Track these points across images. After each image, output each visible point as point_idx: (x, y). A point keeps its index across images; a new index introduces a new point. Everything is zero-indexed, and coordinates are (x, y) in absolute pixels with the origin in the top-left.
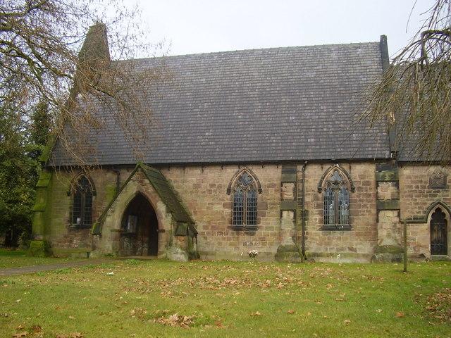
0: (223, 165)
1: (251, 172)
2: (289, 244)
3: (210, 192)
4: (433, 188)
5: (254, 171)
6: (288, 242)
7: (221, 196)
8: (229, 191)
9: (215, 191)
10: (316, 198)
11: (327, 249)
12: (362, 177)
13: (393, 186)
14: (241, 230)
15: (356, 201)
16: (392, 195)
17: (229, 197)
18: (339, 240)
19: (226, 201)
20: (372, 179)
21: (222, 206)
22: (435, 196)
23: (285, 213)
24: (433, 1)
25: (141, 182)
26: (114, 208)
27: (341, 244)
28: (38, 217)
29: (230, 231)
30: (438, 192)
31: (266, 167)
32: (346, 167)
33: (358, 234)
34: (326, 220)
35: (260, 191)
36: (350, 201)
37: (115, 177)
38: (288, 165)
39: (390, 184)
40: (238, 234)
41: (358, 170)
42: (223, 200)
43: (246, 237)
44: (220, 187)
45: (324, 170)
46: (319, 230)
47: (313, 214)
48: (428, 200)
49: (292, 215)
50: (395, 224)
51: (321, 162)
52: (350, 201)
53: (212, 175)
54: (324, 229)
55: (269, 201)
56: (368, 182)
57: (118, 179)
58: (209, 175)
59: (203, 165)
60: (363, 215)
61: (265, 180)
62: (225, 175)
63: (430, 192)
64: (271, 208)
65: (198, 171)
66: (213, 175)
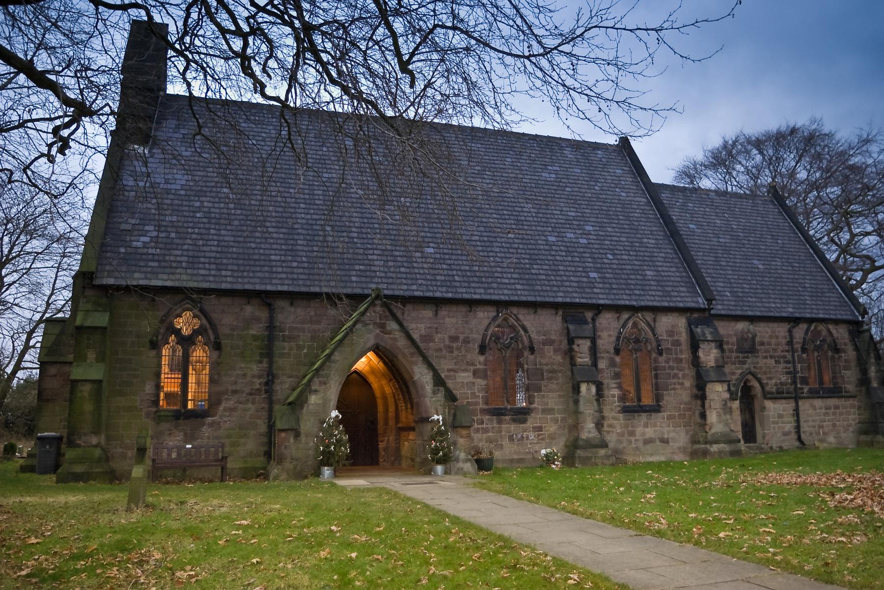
0: (472, 304)
1: (518, 320)
2: (591, 435)
3: (450, 349)
4: (742, 352)
5: (521, 317)
6: (589, 432)
7: (469, 357)
8: (483, 349)
9: (458, 349)
10: (612, 364)
11: (630, 442)
12: (671, 333)
13: (716, 348)
14: (505, 415)
15: (664, 368)
16: (716, 360)
17: (482, 358)
18: (647, 428)
19: (478, 366)
20: (684, 337)
21: (471, 374)
22: (744, 363)
23: (584, 387)
24: (0, 137)
25: (382, 326)
26: (327, 376)
27: (650, 432)
28: (86, 394)
29: (486, 418)
30: (747, 357)
31: (539, 311)
32: (649, 317)
33: (298, 421)
34: (623, 398)
35: (532, 350)
36: (656, 369)
37: (263, 314)
38: (572, 312)
39: (713, 344)
40: (500, 422)
41: (665, 322)
42: (473, 364)
43: (513, 427)
44: (466, 341)
45: (622, 321)
46: (619, 412)
47: (609, 389)
48: (737, 369)
49: (593, 389)
50: (726, 401)
51: (617, 309)
52: (656, 369)
53: (452, 321)
54: (626, 410)
55: (545, 368)
56: (678, 340)
57: (271, 319)
58: (447, 320)
59: (437, 303)
60: (675, 389)
61: (538, 332)
62: (474, 322)
63: (738, 357)
64: (550, 379)
65: (427, 313)
66: (453, 320)
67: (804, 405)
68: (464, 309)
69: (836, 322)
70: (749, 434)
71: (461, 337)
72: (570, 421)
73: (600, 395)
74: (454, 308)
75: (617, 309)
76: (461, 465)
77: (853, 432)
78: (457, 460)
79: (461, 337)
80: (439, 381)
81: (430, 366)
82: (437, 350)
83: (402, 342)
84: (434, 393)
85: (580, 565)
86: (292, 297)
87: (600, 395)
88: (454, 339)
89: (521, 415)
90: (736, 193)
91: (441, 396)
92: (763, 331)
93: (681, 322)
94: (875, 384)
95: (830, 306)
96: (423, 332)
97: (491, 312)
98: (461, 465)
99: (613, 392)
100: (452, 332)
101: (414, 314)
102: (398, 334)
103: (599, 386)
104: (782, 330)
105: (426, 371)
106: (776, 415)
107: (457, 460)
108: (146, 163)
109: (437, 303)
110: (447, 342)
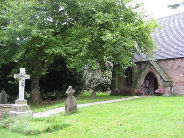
3: (177, 69)
25: (150, 67)
66: (178, 62)
68: (180, 59)
71: (180, 66)
74: (178, 60)
76: (166, 94)
77: (160, 85)
78: (166, 93)
79: (180, 66)
81: (160, 75)
82: (174, 70)
83: (154, 70)
84: (161, 80)
88: (178, 67)
90: (4, 97)
91: (162, 80)
96: (171, 66)
98: (166, 94)
100: (178, 65)
101: (169, 62)
102: (153, 68)
105: (159, 75)
107: (166, 93)
109: (166, 60)
110: (177, 68)
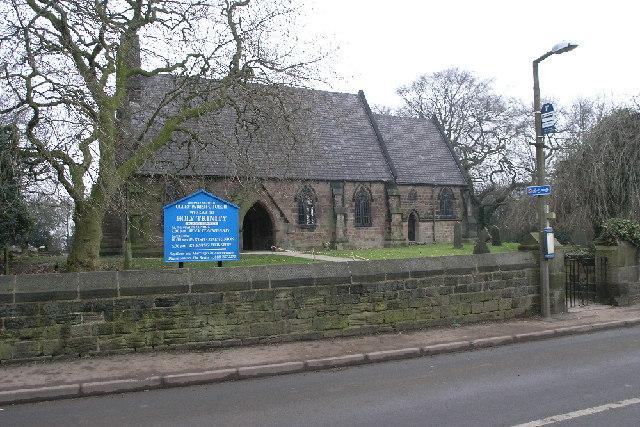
12: (377, 192)
18: (365, 232)
23: (338, 217)
67: (437, 224)
69: (455, 186)
70: (412, 236)
72: (332, 230)
73: (346, 220)
75: (354, 181)
80: (282, 215)
85: (385, 270)
86: (375, 182)
87: (346, 220)
89: (312, 228)
92: (420, 191)
93: (381, 187)
94: (469, 214)
95: (452, 178)
97: (440, 188)
99: (351, 218)
103: (345, 215)
104: (428, 190)
106: (424, 228)
108: (495, 134)
